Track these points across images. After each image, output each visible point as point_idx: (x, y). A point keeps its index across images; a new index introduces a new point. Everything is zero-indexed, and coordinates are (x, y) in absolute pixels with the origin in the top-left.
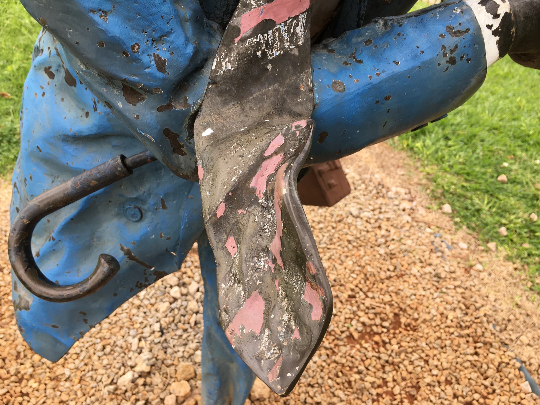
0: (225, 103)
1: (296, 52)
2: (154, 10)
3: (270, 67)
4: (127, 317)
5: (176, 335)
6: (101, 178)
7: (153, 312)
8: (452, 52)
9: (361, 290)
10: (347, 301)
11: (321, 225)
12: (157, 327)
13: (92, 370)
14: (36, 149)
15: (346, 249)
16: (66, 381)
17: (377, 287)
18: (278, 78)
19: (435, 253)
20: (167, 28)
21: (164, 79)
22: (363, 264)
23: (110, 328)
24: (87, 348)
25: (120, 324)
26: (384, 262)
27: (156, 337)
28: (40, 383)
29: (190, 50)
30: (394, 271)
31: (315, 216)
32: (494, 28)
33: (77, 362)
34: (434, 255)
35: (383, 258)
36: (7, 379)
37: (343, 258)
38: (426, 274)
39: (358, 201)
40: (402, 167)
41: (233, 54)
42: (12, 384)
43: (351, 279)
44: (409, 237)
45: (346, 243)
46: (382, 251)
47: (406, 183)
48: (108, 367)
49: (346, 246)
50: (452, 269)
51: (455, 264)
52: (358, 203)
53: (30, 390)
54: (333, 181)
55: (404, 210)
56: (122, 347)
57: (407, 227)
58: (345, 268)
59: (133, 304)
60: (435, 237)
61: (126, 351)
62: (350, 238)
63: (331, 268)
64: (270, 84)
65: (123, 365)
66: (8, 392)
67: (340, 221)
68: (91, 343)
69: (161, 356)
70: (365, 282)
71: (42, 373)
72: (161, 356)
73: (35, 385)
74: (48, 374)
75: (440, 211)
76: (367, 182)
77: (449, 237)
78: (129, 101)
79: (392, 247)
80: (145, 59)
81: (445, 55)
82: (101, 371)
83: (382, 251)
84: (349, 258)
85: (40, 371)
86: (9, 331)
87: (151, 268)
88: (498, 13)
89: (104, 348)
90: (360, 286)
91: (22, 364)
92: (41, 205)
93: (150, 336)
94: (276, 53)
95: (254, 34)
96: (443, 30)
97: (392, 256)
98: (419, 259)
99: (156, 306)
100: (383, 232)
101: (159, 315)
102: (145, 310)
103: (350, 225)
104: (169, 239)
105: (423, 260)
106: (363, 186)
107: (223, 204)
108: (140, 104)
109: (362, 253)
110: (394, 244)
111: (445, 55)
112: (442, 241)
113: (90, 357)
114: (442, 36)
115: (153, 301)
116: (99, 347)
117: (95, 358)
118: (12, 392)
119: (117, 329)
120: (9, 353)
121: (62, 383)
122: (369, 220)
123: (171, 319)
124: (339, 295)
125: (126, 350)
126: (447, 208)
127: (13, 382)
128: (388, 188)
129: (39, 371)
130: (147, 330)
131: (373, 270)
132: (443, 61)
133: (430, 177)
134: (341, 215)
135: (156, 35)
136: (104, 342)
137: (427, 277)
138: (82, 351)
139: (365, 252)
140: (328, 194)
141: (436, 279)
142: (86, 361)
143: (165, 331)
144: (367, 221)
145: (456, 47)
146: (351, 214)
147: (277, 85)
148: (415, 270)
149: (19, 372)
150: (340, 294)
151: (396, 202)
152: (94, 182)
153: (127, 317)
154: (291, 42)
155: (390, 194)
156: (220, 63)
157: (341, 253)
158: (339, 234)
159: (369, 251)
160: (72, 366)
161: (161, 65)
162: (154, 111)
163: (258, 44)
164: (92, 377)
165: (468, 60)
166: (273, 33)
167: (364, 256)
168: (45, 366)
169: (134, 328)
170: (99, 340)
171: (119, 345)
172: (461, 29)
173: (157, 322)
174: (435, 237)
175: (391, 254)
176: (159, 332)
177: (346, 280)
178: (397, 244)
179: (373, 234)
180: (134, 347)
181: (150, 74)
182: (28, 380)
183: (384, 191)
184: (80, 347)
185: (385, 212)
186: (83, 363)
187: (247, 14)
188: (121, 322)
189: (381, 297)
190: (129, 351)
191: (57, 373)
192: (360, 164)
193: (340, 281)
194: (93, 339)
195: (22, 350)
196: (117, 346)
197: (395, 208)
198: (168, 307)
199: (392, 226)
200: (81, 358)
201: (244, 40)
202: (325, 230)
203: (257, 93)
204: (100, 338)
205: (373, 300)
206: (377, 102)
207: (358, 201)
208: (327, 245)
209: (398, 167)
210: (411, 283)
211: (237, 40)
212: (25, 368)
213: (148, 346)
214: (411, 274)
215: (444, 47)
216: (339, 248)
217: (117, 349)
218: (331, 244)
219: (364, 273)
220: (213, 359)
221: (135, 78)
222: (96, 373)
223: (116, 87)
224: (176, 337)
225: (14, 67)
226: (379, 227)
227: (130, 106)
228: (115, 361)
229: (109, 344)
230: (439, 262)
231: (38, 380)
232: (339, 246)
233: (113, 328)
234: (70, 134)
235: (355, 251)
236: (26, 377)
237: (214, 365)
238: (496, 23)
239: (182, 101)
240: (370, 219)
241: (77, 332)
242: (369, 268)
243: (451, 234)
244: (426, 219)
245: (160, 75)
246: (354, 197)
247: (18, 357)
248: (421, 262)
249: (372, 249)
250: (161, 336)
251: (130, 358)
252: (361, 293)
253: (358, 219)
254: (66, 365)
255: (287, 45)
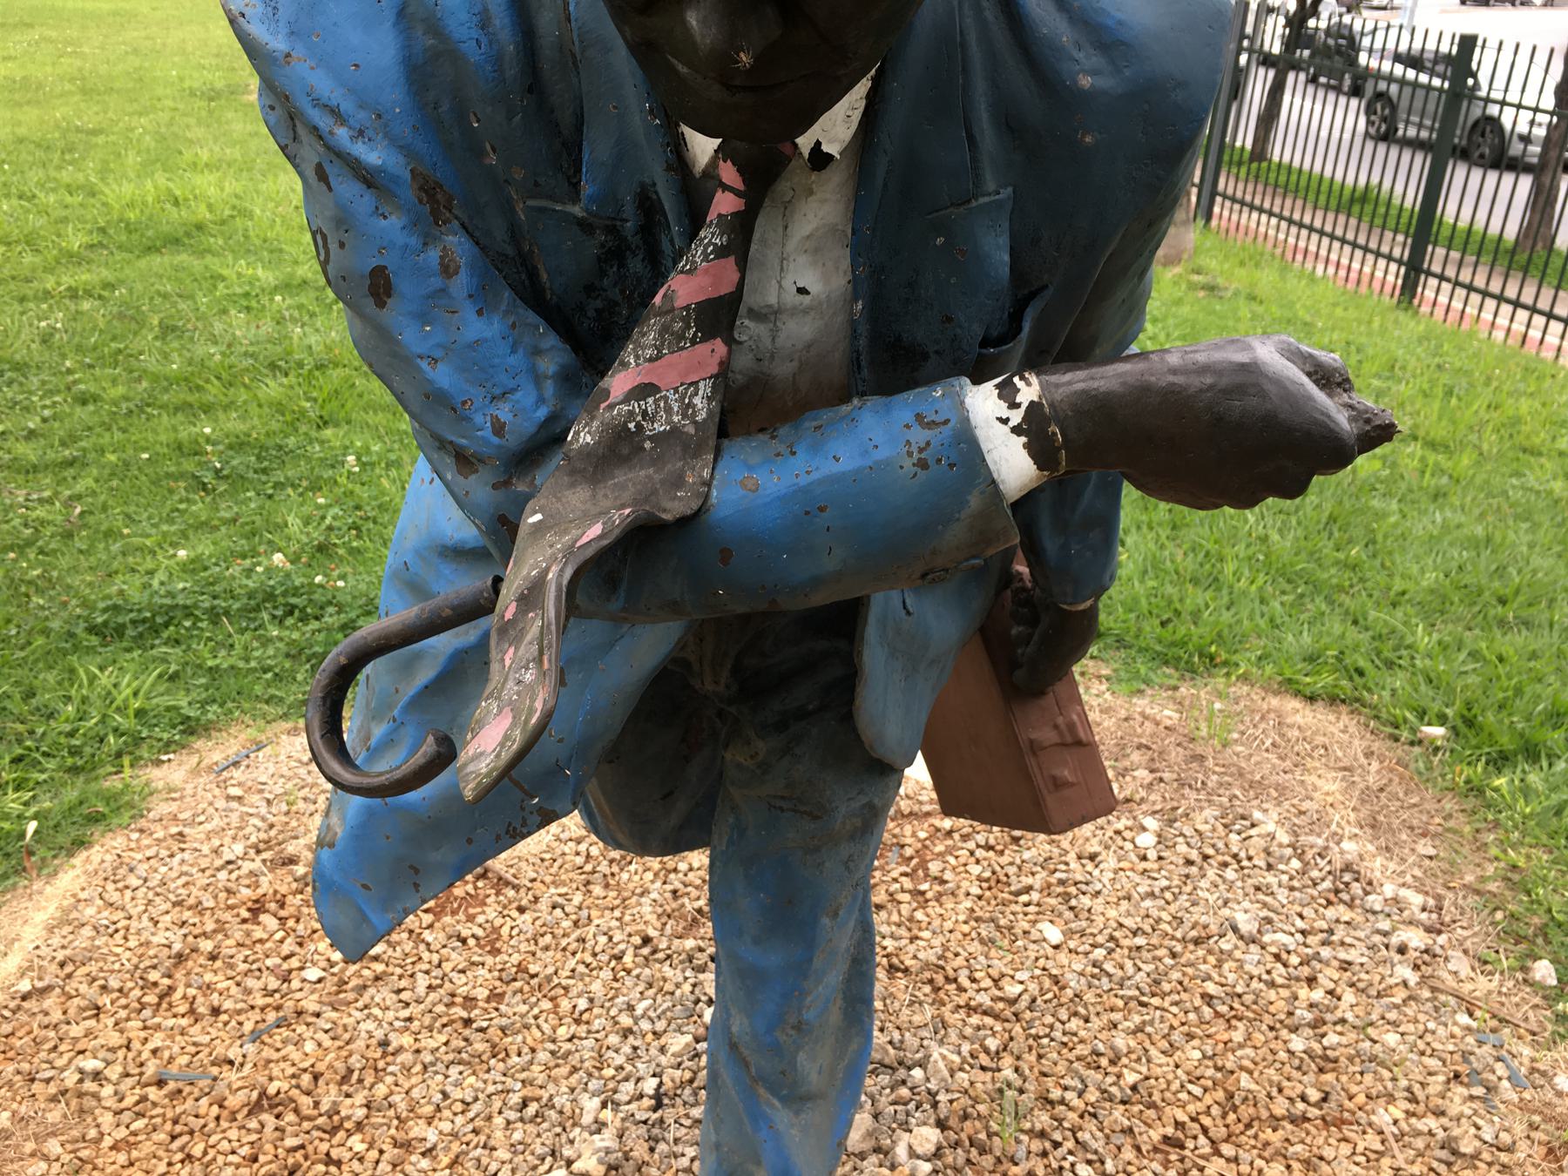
0: (573, 485)
1: (691, 430)
2: (497, 361)
3: (648, 445)
4: (592, 1049)
5: (687, 1116)
6: (459, 606)
7: (654, 1052)
8: (921, 450)
9: (1205, 1130)
10: (1156, 1150)
11: (1140, 941)
12: (650, 1085)
13: (484, 1147)
14: (402, 566)
15: (1192, 1016)
16: (423, 1154)
17: (1256, 1137)
18: (657, 461)
19: (1467, 1086)
20: (512, 384)
21: (500, 447)
22: (1229, 1065)
23: (552, 1064)
24: (489, 1096)
25: (574, 1060)
26: (1296, 1074)
27: (641, 1110)
28: (371, 1147)
29: (542, 413)
30: (1318, 1105)
31: (1129, 914)
32: (1011, 424)
33: (459, 1120)
34: (1459, 1091)
35: (1296, 1062)
36: (310, 1119)
37: (1176, 1036)
38: (1418, 1134)
39: (1268, 899)
40: (1435, 836)
41: (595, 424)
42: (315, 1133)
43: (1183, 1096)
44: (1395, 1024)
45: (1198, 1002)
46: (1298, 1044)
47: (1431, 881)
48: (520, 1148)
49: (1196, 1009)
50: (1505, 1138)
51: (1520, 1129)
52: (1265, 905)
53: (347, 1155)
54: (1066, 774)
55: (1402, 950)
56: (561, 1112)
57: (1399, 996)
58: (1177, 1066)
59: (616, 1023)
60: (1480, 1043)
61: (568, 1124)
62: (1211, 988)
63: (1133, 1056)
64: (642, 468)
65: (553, 1154)
66: (302, 1147)
67: (1197, 942)
68: (500, 1087)
69: (640, 1151)
70: (1224, 1116)
71: (382, 1125)
72: (640, 1151)
73: (360, 1147)
74: (393, 1131)
75: (1519, 976)
76: (1309, 855)
77: (1527, 1051)
78: (460, 473)
79: (1332, 1039)
80: (478, 419)
81: (910, 454)
82: (503, 1154)
83: (1298, 1044)
84: (1196, 1042)
85: (381, 1120)
86: (346, 1020)
87: (533, 797)
88: (1018, 400)
89: (525, 1104)
90: (1206, 1121)
91: (348, 1096)
92: (370, 638)
93: (629, 1103)
94: (660, 427)
95: (626, 400)
96: (908, 417)
97: (1326, 1062)
98: (1409, 1090)
99: (663, 1041)
100: (1318, 995)
101: (663, 1060)
102: (636, 1043)
103: (1223, 957)
104: (560, 741)
105: (1420, 1095)
106: (1296, 864)
107: (514, 604)
108: (473, 477)
109: (1238, 1036)
110: (1341, 1034)
111: (910, 454)
112: (1499, 1059)
113: (489, 1118)
114: (907, 426)
115: (660, 1025)
116: (515, 1099)
117: (499, 1121)
118: (310, 1148)
119: (564, 1070)
120: (331, 1066)
121: (413, 1158)
122: (1284, 956)
123: (688, 1075)
124: (1136, 1130)
125: (571, 1119)
126: (1544, 971)
127: (318, 1128)
128: (1370, 883)
129: (377, 1119)
130: (628, 1088)
131: (1253, 1087)
132: (908, 463)
133: (1516, 877)
134: (1205, 927)
135: (497, 391)
136: (528, 1092)
137: (1420, 1143)
138: (476, 1099)
139: (1249, 1037)
140: (1051, 801)
141: (1444, 1154)
142: (479, 1123)
143: (666, 1101)
144: (1277, 957)
145: (928, 444)
146: (1235, 929)
147: (651, 471)
148: (1384, 1116)
149: (338, 1113)
150: (1139, 1127)
151: (1385, 925)
152: (448, 612)
153: (592, 1049)
154: (684, 416)
155: (1374, 901)
156: (577, 433)
157: (1176, 1023)
158: (1184, 974)
159: (1259, 1038)
160: (446, 1126)
161: (499, 428)
162: (489, 488)
163: (631, 413)
164: (479, 1160)
165: (951, 466)
166: (656, 401)
167: (1241, 1046)
168: (391, 1113)
169: (601, 1078)
170: (519, 1085)
171: (558, 1106)
172: (938, 419)
173: (654, 1075)
174: (1480, 1043)
175: (1326, 1058)
176: (651, 1097)
177: (1168, 1095)
178: (1353, 1036)
179: (1285, 993)
180: (587, 1119)
181: (483, 438)
182: (349, 1134)
183: (1356, 888)
184: (476, 1090)
185: (1342, 944)
186: (470, 1127)
187: (622, 374)
188: (577, 1055)
189: (1259, 1163)
190: (574, 1125)
191: (412, 1135)
192: (1306, 805)
193: (1150, 1095)
194: (509, 1080)
195: (358, 1065)
196: (553, 1107)
197: (1377, 939)
198: (687, 1045)
199: (1352, 985)
200: (471, 1114)
201: (611, 407)
202: (1146, 955)
203: (621, 476)
204: (523, 1082)
205: (1233, 1165)
206: (807, 513)
207: (1268, 899)
208: (1143, 994)
209: (1424, 835)
210: (1360, 1149)
211: (603, 405)
212: (352, 1106)
213: (618, 1123)
214: (1370, 1125)
215: (908, 442)
216: (1174, 1009)
217: (553, 1114)
218: (1153, 995)
219: (1225, 1090)
220: (718, 1146)
221: (464, 442)
222: (490, 1156)
223: (448, 453)
224: (687, 1122)
225: (1408, 715)
226: (1311, 981)
227: (460, 479)
228: (538, 1140)
229: (538, 1100)
230: (1468, 1112)
231: (368, 1139)
232: (1176, 1004)
233: (557, 1066)
234: (450, 543)
235: (1218, 1028)
236: (347, 1125)
237: (720, 1164)
238: (1016, 417)
239: (528, 479)
240: (1289, 952)
241: (399, 907)
242: (1245, 1081)
243: (1535, 1045)
244: (1466, 988)
245: (495, 440)
246: (1258, 889)
247: (345, 1079)
248: (1413, 1099)
249: (1272, 1035)
250: (655, 1111)
251: (572, 1142)
252: (1202, 1140)
253: (1253, 948)
254: (436, 1121)
255: (676, 419)
